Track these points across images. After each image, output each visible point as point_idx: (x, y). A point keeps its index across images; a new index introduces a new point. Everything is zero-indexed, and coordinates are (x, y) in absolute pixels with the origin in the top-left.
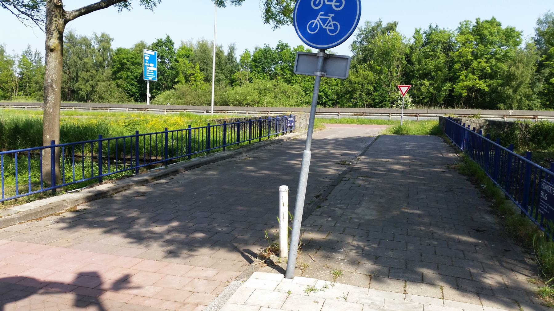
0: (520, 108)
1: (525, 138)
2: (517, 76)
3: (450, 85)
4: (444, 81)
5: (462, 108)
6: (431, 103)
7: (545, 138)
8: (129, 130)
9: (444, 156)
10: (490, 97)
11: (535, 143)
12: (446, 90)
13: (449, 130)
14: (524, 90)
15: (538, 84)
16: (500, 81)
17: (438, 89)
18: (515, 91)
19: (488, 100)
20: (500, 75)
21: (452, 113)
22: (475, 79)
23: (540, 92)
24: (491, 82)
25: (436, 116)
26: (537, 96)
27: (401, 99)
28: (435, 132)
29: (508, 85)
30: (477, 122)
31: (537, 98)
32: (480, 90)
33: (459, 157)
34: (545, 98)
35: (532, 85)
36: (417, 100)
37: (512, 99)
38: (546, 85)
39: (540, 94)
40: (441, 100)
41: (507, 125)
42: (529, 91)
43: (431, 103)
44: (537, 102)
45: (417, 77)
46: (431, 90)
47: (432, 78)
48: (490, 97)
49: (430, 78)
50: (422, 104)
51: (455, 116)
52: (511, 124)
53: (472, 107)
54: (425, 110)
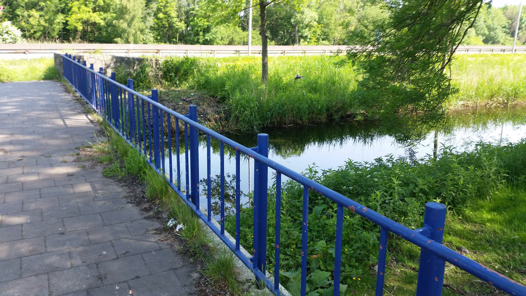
0: (136, 42)
1: (157, 75)
2: (129, 10)
3: (63, 17)
4: (57, 12)
5: (80, 42)
6: (45, 37)
7: (176, 73)
8: (323, 31)
9: (68, 122)
10: (107, 31)
11: (167, 80)
12: (59, 23)
13: (69, 72)
14: (137, 24)
15: (148, 18)
16: (114, 15)
17: (50, 22)
18: (129, 26)
19: (104, 34)
20: (113, 8)
21: (72, 49)
22: (89, 12)
23: (151, 27)
24: (105, 15)
25: (51, 53)
26: (149, 31)
27: (7, 33)
28: (51, 76)
29: (121, 18)
30: (102, 59)
31: (150, 33)
32: (94, 24)
33: (92, 122)
34: (156, 33)
35: (144, 19)
36: (28, 34)
37: (128, 33)
38: (156, 20)
39: (152, 28)
40: (55, 34)
41: (137, 62)
42: (142, 25)
43: (45, 37)
44: (150, 36)
45: (22, 6)
46: (43, 23)
47: (42, 9)
48: (107, 31)
49: (40, 9)
50: (34, 38)
51: (73, 53)
52: (140, 61)
53: (91, 41)
54: (38, 45)
